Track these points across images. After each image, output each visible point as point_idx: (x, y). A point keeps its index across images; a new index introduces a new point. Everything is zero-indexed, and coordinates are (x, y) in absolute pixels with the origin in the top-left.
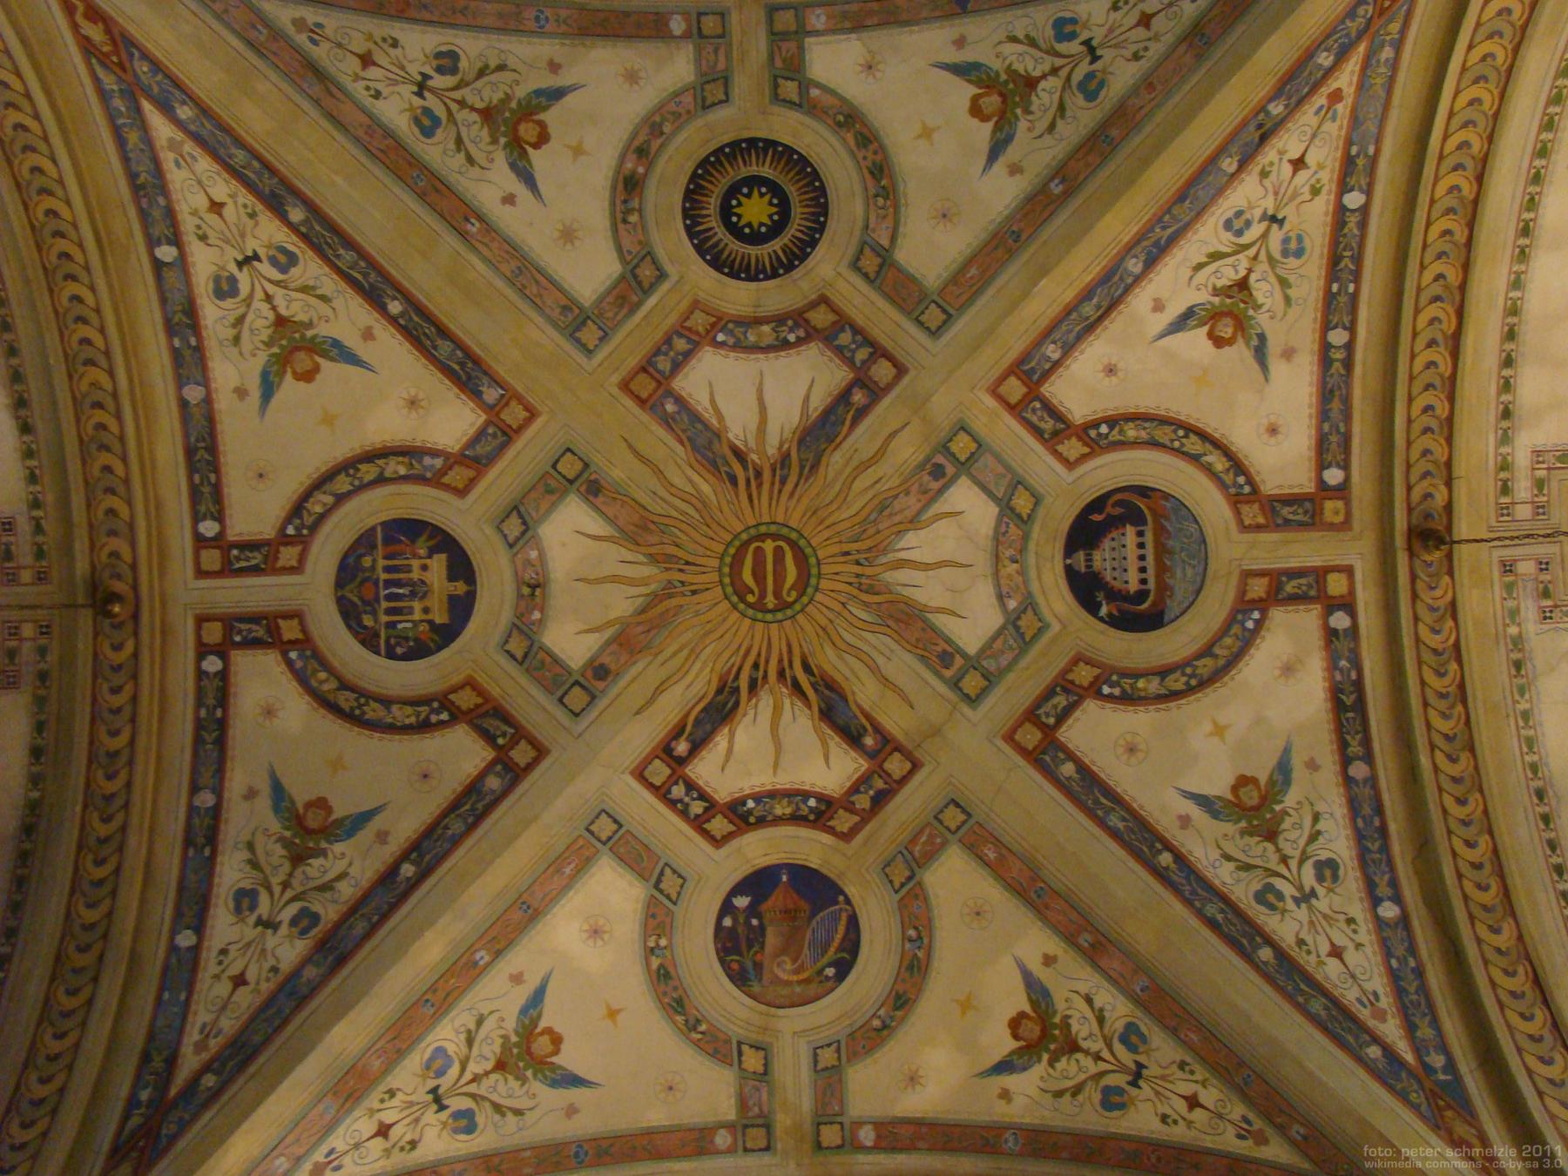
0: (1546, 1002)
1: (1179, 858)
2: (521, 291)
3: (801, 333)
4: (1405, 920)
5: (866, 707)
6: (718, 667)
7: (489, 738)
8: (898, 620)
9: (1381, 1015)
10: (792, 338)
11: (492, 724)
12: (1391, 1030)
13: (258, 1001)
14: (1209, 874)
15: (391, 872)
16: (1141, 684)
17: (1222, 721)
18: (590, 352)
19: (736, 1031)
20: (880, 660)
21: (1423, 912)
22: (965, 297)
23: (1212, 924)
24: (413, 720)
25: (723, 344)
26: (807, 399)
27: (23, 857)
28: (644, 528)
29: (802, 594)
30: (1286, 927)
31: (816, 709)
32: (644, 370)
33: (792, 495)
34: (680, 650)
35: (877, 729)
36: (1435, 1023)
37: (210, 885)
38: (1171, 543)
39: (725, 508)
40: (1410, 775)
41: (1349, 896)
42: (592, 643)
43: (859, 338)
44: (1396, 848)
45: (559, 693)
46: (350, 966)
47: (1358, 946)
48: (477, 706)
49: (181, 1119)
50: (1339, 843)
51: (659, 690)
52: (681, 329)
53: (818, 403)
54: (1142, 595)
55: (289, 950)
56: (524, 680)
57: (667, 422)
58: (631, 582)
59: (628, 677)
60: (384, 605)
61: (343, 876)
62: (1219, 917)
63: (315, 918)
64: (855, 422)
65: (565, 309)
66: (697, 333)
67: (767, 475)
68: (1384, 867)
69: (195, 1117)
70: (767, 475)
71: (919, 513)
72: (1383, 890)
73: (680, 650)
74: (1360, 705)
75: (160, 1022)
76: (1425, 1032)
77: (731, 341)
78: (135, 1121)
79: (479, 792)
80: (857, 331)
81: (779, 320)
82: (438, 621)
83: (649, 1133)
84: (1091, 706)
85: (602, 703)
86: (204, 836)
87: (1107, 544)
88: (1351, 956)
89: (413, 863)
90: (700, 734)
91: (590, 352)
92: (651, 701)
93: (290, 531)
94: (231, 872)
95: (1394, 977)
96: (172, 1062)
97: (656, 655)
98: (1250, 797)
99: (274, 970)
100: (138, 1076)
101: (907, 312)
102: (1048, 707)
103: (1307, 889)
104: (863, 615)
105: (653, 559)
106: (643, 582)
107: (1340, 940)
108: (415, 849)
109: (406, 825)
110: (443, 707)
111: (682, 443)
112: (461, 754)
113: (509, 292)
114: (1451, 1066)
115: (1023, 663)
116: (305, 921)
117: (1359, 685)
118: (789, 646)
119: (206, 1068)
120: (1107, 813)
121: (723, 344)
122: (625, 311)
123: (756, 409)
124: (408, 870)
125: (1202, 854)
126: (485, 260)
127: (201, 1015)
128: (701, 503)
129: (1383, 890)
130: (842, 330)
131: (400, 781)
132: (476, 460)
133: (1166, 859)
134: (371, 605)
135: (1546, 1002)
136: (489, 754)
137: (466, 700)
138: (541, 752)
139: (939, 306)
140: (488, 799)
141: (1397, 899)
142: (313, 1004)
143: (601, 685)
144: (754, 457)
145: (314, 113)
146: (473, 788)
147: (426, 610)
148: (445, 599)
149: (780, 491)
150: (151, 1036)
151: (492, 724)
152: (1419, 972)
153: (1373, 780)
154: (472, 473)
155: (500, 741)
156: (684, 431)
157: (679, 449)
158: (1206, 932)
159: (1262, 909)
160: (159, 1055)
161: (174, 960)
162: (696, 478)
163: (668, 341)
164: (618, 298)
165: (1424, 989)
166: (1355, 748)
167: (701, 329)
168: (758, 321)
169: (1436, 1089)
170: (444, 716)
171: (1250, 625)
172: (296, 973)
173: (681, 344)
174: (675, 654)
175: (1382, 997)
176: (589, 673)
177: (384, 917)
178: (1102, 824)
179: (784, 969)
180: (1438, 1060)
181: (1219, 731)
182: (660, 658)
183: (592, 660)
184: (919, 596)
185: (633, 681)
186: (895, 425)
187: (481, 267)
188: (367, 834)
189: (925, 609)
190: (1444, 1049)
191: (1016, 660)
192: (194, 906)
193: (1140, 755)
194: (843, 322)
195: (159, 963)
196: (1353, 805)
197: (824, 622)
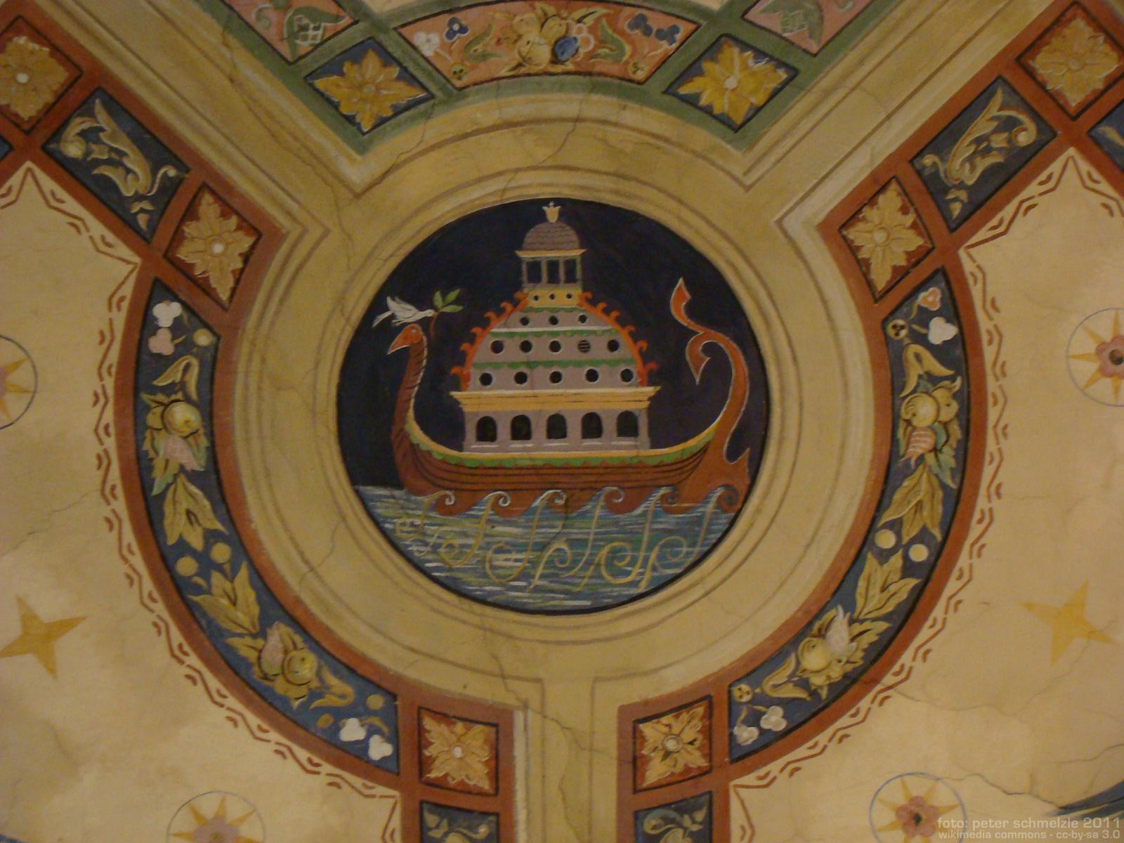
11: (962, 167)
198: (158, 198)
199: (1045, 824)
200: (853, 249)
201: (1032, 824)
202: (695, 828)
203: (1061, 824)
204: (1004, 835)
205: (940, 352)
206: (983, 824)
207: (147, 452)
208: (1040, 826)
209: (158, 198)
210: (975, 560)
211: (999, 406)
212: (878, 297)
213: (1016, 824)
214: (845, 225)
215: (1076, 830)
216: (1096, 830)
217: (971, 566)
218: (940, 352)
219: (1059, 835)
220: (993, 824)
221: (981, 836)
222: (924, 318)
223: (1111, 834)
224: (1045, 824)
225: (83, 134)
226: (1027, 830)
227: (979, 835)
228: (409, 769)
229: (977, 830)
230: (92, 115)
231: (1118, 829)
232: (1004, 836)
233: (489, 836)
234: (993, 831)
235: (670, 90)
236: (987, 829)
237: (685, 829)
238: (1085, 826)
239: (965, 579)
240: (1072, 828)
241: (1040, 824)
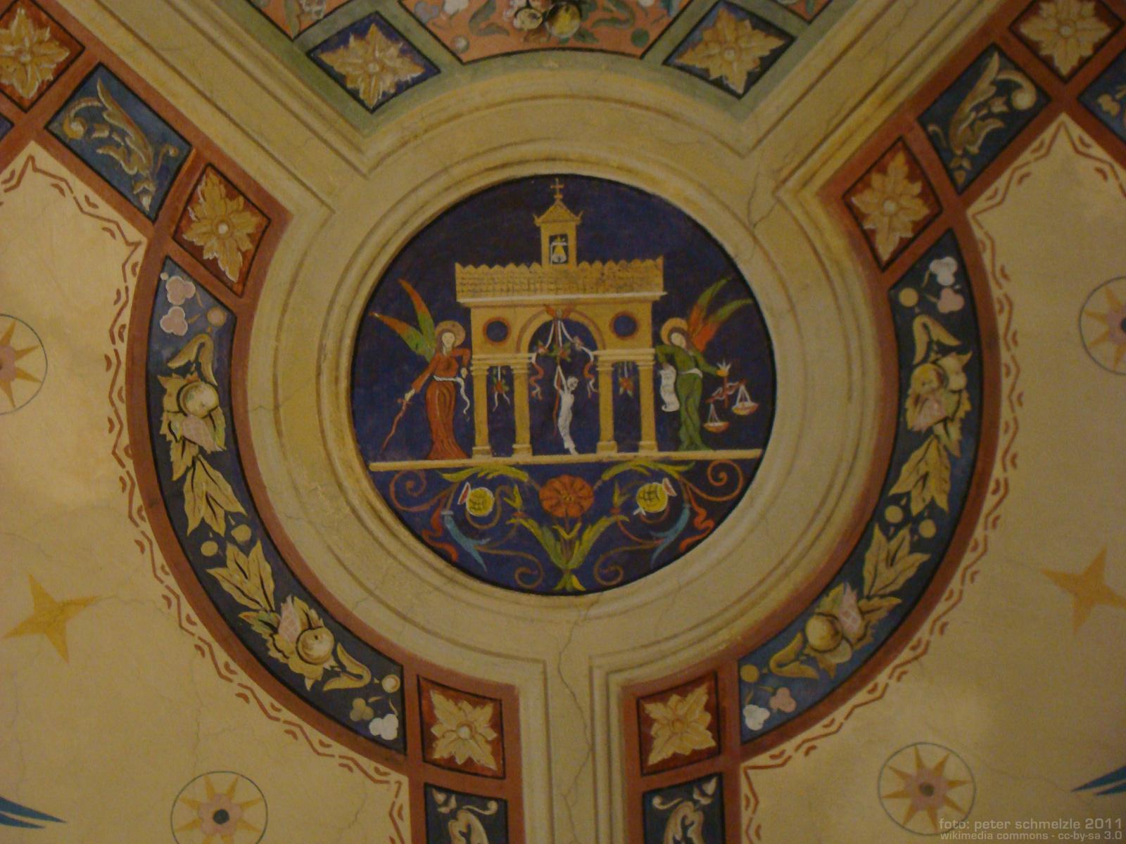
11: (970, 128)
24: (951, 363)
48: (916, 171)
60: (607, 450)
110: (916, 275)
132: (168, 174)
137: (895, 208)
147: (625, 326)
151: (970, 128)
155: (1025, 99)
198: (167, 181)
199: (1047, 825)
200: (856, 217)
201: (1034, 825)
202: (705, 801)
203: (1063, 825)
204: (1006, 836)
205: (947, 321)
206: (985, 825)
207: (164, 436)
208: (1042, 827)
209: (167, 181)
210: (893, 682)
211: (1012, 377)
212: (884, 267)
213: (1018, 825)
214: (852, 190)
215: (1078, 831)
216: (1097, 831)
217: (887, 685)
218: (947, 321)
219: (1061, 836)
220: (995, 825)
221: (982, 836)
222: (935, 304)
223: (1113, 835)
224: (1047, 825)
225: (91, 113)
226: (1029, 831)
227: (980, 836)
228: (412, 748)
229: (979, 831)
230: (94, 94)
231: (1120, 830)
232: (1006, 837)
233: (498, 812)
234: (995, 832)
235: (670, 61)
236: (990, 830)
237: (695, 802)
238: (1087, 827)
239: (877, 694)
240: (1074, 830)
241: (1042, 824)
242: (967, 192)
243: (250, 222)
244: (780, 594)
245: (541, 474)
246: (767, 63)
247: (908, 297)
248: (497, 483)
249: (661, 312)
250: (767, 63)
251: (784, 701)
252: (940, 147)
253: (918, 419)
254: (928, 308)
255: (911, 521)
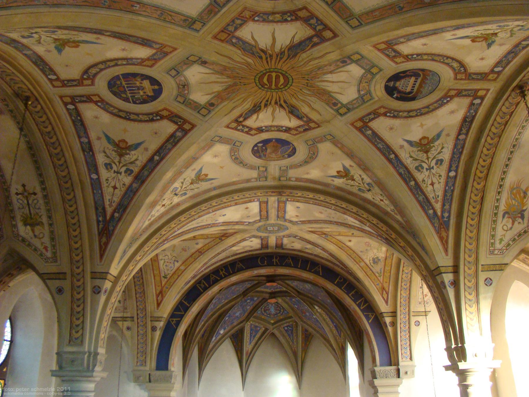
0: (481, 204)
1: (396, 156)
2: (164, 20)
3: (294, 18)
4: (456, 177)
5: (305, 113)
6: (254, 102)
7: (176, 123)
8: (319, 94)
9: (437, 202)
10: (289, 19)
11: (175, 119)
12: (438, 207)
13: (122, 193)
14: (404, 161)
15: (151, 159)
16: (400, 114)
17: (424, 123)
18: (198, 31)
19: (257, 165)
20: (312, 104)
21: (462, 174)
22: (370, 21)
23: (400, 174)
24: (148, 119)
25: (257, 21)
26: (294, 37)
27: (33, 155)
28: (225, 70)
29: (284, 87)
30: (419, 177)
31: (287, 111)
32: (222, 31)
33: (284, 62)
34: (241, 98)
35: (307, 117)
36: (450, 206)
37: (96, 162)
38: (426, 81)
39: (257, 65)
40: (478, 140)
41: (443, 170)
42: (208, 97)
43: (319, 22)
44: (463, 157)
45: (198, 110)
46: (146, 183)
47: (439, 183)
48: (169, 115)
49: (113, 226)
50: (446, 155)
51: (232, 109)
52: (240, 16)
53: (297, 40)
54: (410, 93)
55: (128, 180)
56: (185, 108)
57: (234, 45)
58: (222, 83)
59: (220, 107)
60: (128, 92)
61: (136, 160)
62: (403, 172)
63: (132, 171)
64: (312, 47)
65: (185, 20)
66: (246, 18)
67: (274, 56)
68: (457, 162)
69: (117, 225)
70: (274, 56)
71: (333, 70)
72: (454, 168)
73: (241, 98)
74: (471, 122)
75: (96, 199)
76: (447, 207)
77: (261, 19)
78: (101, 226)
79: (175, 137)
80: (318, 19)
81: (284, 13)
82: (149, 94)
83: (233, 182)
84: (382, 118)
85: (213, 113)
86: (88, 149)
87: (403, 81)
88: (436, 186)
89: (158, 156)
90: (247, 116)
91: (198, 31)
92: (231, 111)
93: (85, 77)
94: (101, 159)
95: (445, 191)
96: (104, 209)
97: (231, 100)
98: (425, 142)
99: (124, 184)
100: (97, 215)
101: (343, 19)
102: (367, 118)
103: (431, 166)
104: (308, 92)
105: (228, 77)
106: (226, 82)
107: (435, 180)
108: (158, 152)
109: (153, 146)
110: (157, 115)
111: (240, 49)
112: (167, 128)
113: (158, 22)
114: (449, 217)
115: (362, 107)
116: (129, 172)
117: (474, 117)
118: (280, 98)
119: (114, 211)
120: (378, 144)
121: (257, 21)
122: (212, 15)
123: (271, 39)
124: (157, 158)
125: (404, 156)
126: (145, 16)
127: (107, 198)
128: (248, 64)
129: (454, 168)
130: (312, 18)
131: (150, 136)
132: (155, 59)
133: (392, 156)
134: (125, 92)
135: (481, 204)
136: (176, 127)
137: (165, 113)
138: (193, 126)
139: (358, 20)
140: (178, 139)
141: (456, 171)
142: (138, 194)
143: (212, 108)
144: (270, 52)
145: (45, 9)
146: (173, 135)
147: (145, 93)
148: (152, 91)
149: (279, 61)
150: (95, 203)
151: (175, 119)
152: (453, 191)
153: (465, 140)
154: (153, 62)
155: (179, 123)
156: (240, 47)
157: (239, 52)
158: (398, 176)
159: (416, 171)
160: (100, 208)
161: (93, 181)
162: (245, 58)
163: (233, 21)
164: (208, 11)
165: (452, 195)
166: (464, 131)
167: (247, 16)
168: (274, 13)
169: (442, 223)
170: (158, 118)
171: (445, 101)
172: (131, 186)
173: (238, 22)
174: (238, 100)
175: (440, 197)
176: (207, 105)
177: (152, 170)
178: (376, 146)
179: (273, 155)
180: (446, 215)
181: (422, 125)
182: (233, 101)
183: (208, 102)
184: (329, 89)
185: (224, 106)
186: (330, 50)
187: (143, 19)
188: (141, 149)
189: (330, 92)
190: (449, 212)
191: (359, 106)
192: (93, 167)
193: (394, 130)
194: (312, 16)
195: (89, 184)
196: (455, 146)
197: (293, 93)
242: (168, 119)
243: (353, 26)
244: (116, 106)
245: (124, 87)
246: (180, 102)
247: (155, 115)
248: (121, 83)
249: (147, 95)
250: (180, 102)
251: (102, 106)
252: (173, 116)
253: (140, 116)
254: (154, 116)
255: (128, 116)
